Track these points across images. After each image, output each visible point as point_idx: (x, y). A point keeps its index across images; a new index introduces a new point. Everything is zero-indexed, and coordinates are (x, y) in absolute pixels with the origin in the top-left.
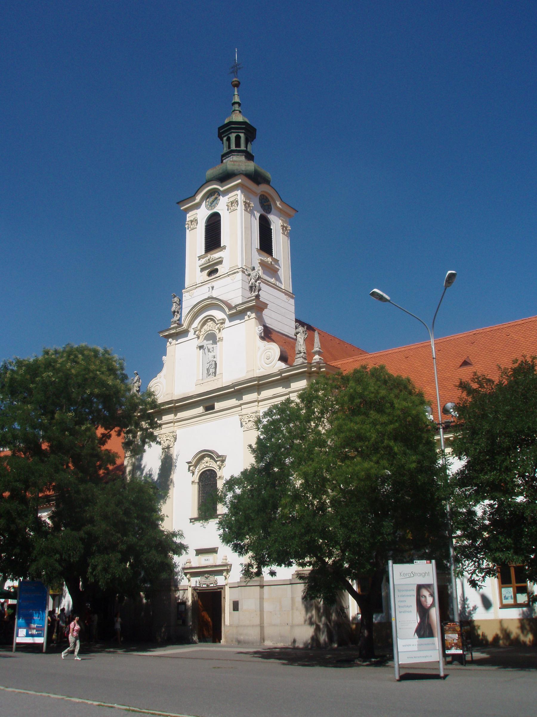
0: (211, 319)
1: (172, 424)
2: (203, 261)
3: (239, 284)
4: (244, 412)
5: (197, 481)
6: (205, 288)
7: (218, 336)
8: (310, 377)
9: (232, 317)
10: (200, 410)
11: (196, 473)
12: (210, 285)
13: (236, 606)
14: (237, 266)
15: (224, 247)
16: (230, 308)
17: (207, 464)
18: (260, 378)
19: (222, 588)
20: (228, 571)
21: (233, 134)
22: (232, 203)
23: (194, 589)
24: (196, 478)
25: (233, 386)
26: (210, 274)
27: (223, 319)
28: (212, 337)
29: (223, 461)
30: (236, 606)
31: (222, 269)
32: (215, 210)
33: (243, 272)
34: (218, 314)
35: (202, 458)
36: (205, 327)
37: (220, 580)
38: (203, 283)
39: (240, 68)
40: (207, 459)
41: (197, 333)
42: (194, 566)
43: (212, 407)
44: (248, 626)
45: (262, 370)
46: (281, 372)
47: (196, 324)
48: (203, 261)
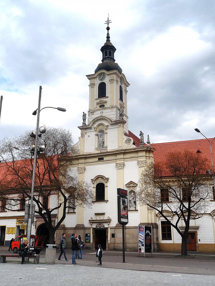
0: (102, 124)
1: (84, 164)
2: (98, 101)
3: (115, 113)
4: (79, 166)
5: (95, 187)
6: (99, 112)
7: (105, 132)
8: (146, 152)
9: (111, 125)
10: (97, 159)
11: (95, 184)
12: (101, 111)
13: (113, 236)
14: (114, 105)
15: (108, 97)
16: (111, 121)
17: (100, 181)
18: (125, 150)
19: (107, 228)
20: (110, 222)
21: (108, 50)
22: (112, 80)
23: (93, 229)
24: (95, 186)
25: (113, 152)
26: (100, 107)
27: (108, 125)
28: (102, 131)
29: (107, 180)
30: (113, 236)
31: (106, 106)
32: (103, 81)
33: (116, 108)
34: (106, 123)
35: (98, 178)
36: (99, 127)
37: (106, 226)
38: (98, 110)
39: (110, 22)
40: (100, 179)
41: (96, 129)
42: (94, 219)
43: (102, 159)
44: (120, 243)
45: (125, 147)
46: (135, 149)
47: (95, 126)
48: (98, 101)
